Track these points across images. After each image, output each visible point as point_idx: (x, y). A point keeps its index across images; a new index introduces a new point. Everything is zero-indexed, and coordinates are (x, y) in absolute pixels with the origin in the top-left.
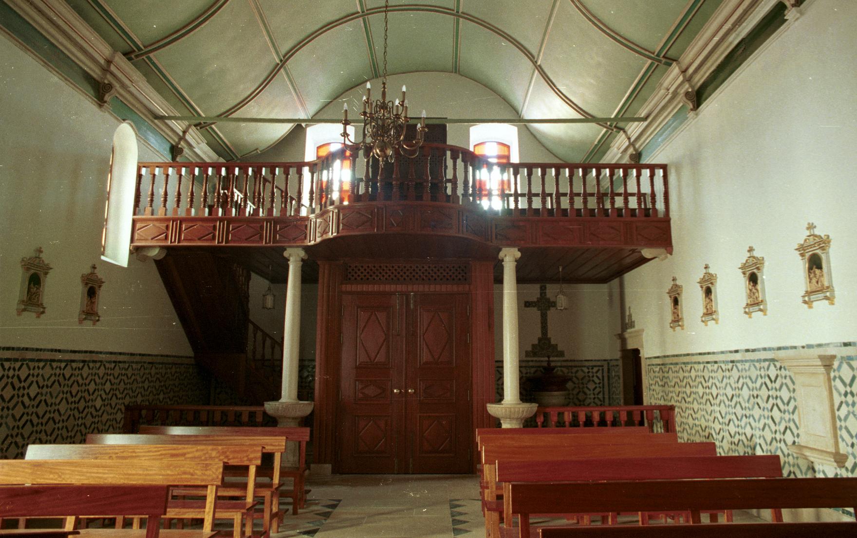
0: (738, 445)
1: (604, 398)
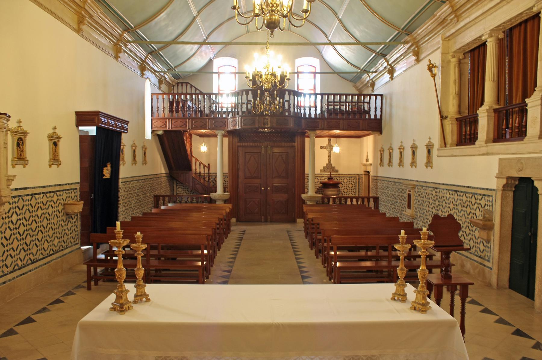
0: (453, 208)
1: (356, 191)
